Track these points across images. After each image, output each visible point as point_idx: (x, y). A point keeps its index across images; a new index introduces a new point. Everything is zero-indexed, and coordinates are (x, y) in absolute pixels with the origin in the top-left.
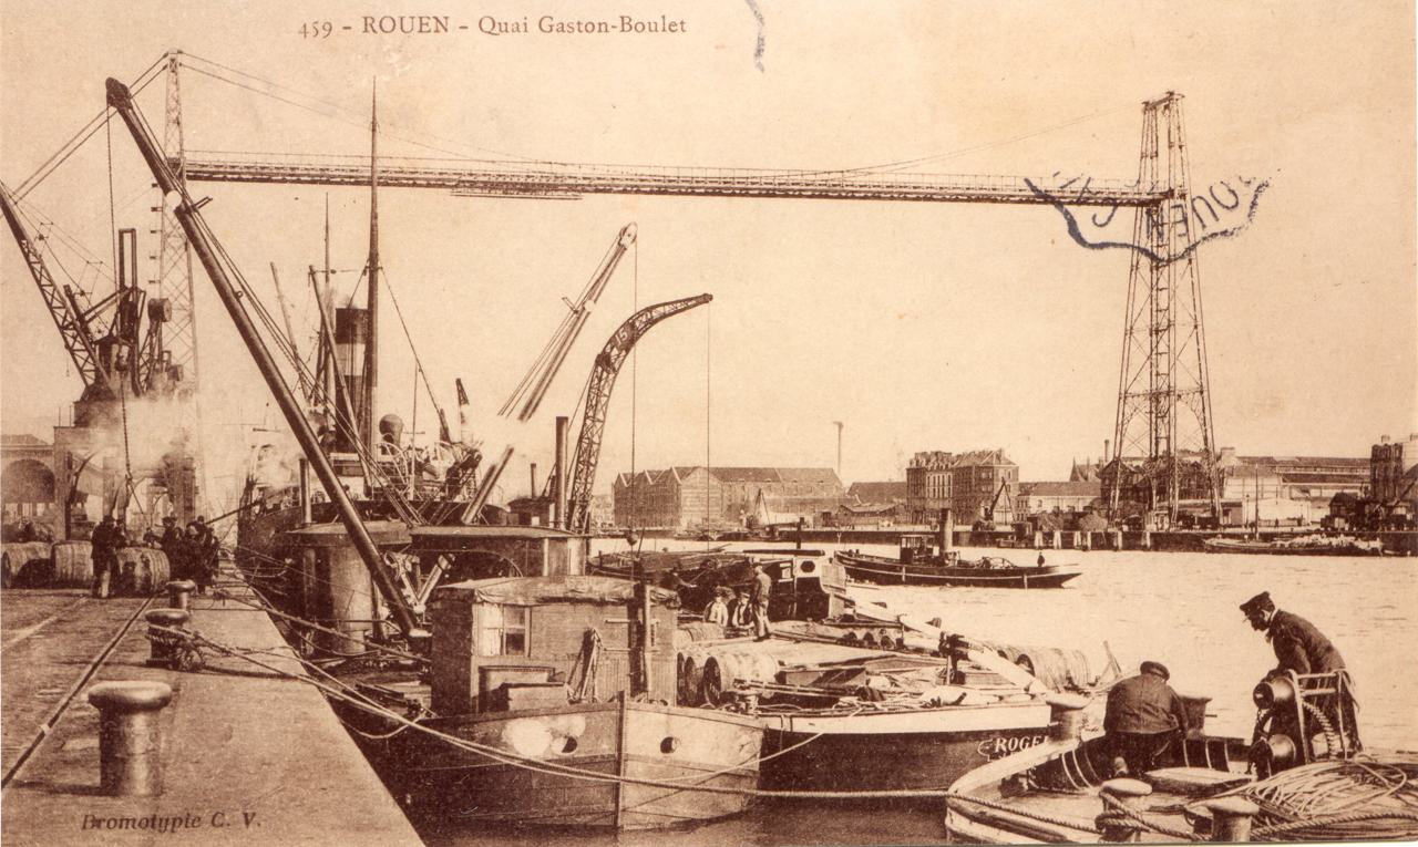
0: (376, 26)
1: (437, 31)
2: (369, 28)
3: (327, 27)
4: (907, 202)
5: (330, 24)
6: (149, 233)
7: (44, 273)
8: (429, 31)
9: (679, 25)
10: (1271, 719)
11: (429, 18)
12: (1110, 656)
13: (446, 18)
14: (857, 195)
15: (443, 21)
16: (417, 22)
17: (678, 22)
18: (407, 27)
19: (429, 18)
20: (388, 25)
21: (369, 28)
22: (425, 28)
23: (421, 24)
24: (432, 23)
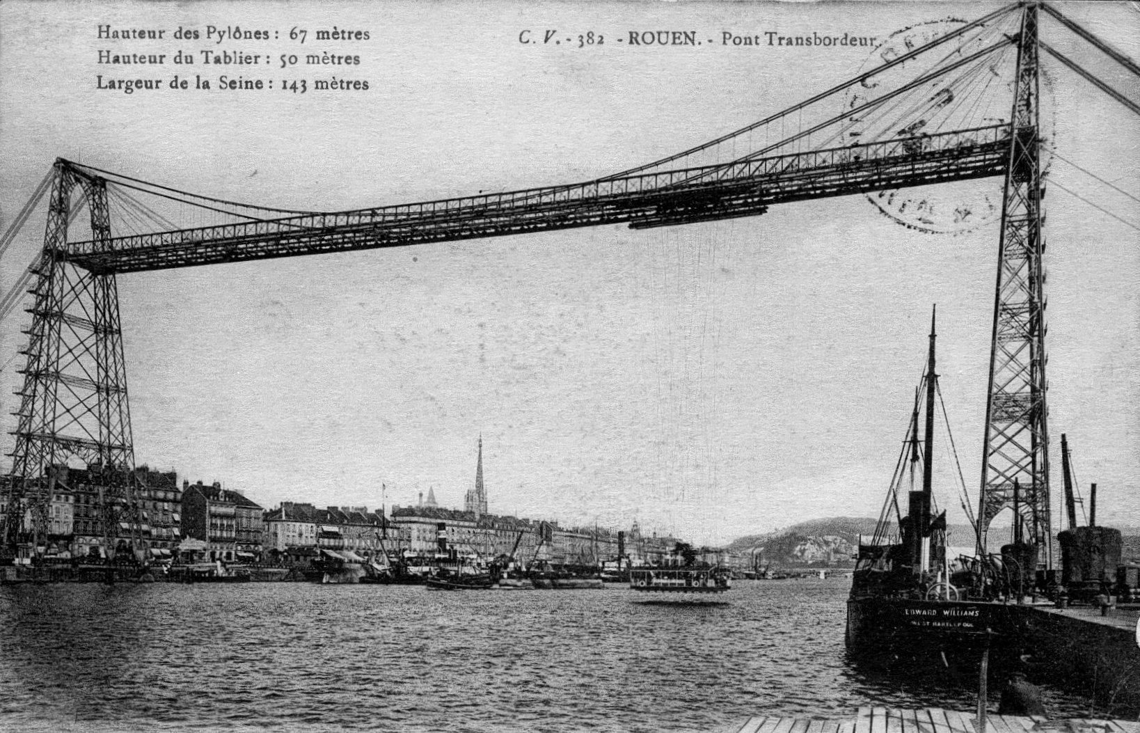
0: (639, 39)
1: (686, 43)
2: (634, 41)
3: (294, 36)
4: (345, 210)
5: (292, 38)
6: (934, 302)
7: (113, 282)
8: (681, 43)
9: (331, 59)
10: (762, 549)
11: (681, 33)
12: (480, 486)
13: (693, 33)
14: (592, 220)
15: (691, 36)
16: (671, 36)
17: (253, 56)
18: (663, 39)
19: (681, 33)
20: (648, 38)
21: (634, 41)
22: (677, 41)
23: (674, 38)
24: (683, 37)
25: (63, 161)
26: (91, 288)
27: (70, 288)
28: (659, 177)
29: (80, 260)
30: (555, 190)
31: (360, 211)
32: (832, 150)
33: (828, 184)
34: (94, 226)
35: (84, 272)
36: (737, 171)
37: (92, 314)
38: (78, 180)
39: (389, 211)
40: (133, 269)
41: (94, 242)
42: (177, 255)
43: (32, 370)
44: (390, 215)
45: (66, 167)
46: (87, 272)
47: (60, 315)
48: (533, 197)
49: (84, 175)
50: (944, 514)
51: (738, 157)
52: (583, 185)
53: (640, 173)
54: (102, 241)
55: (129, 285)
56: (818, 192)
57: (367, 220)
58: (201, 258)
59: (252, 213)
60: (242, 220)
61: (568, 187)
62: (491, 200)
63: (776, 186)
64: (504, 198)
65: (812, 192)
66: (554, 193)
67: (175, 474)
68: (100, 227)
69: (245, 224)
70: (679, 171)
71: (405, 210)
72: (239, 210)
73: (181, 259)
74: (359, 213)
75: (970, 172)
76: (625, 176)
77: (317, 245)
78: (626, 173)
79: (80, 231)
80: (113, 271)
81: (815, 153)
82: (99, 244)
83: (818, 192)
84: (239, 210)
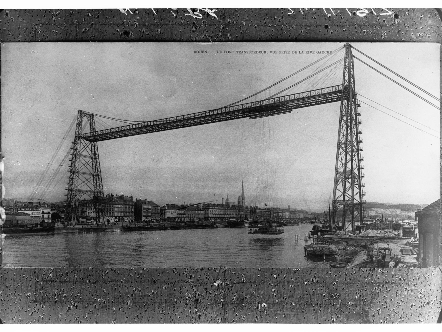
25: (81, 111)
26: (90, 146)
27: (89, 146)
28: (328, 89)
29: (87, 139)
30: (210, 111)
31: (160, 120)
32: (289, 95)
33: (333, 98)
34: (91, 128)
35: (87, 142)
36: (306, 94)
37: (91, 154)
38: (85, 115)
39: (164, 120)
40: (101, 140)
41: (91, 133)
42: (155, 128)
43: (72, 171)
44: (200, 115)
45: (80, 112)
46: (88, 142)
47: (80, 155)
48: (204, 114)
49: (87, 114)
50: (289, 206)
51: (267, 97)
52: (218, 109)
53: (233, 105)
54: (93, 132)
55: (102, 145)
56: (330, 101)
57: (158, 123)
58: (189, 124)
59: (131, 122)
60: (129, 124)
61: (213, 110)
62: (192, 115)
63: (337, 95)
64: (195, 114)
65: (328, 101)
66: (210, 112)
67: (440, 323)
68: (92, 128)
69: (130, 125)
70: (324, 88)
71: (169, 119)
72: (128, 122)
73: (169, 127)
74: (157, 121)
75: (336, 100)
76: (229, 106)
77: (229, 117)
78: (230, 105)
79: (86, 130)
80: (96, 141)
81: (284, 96)
82: (92, 133)
83: (330, 101)
84: (128, 122)
